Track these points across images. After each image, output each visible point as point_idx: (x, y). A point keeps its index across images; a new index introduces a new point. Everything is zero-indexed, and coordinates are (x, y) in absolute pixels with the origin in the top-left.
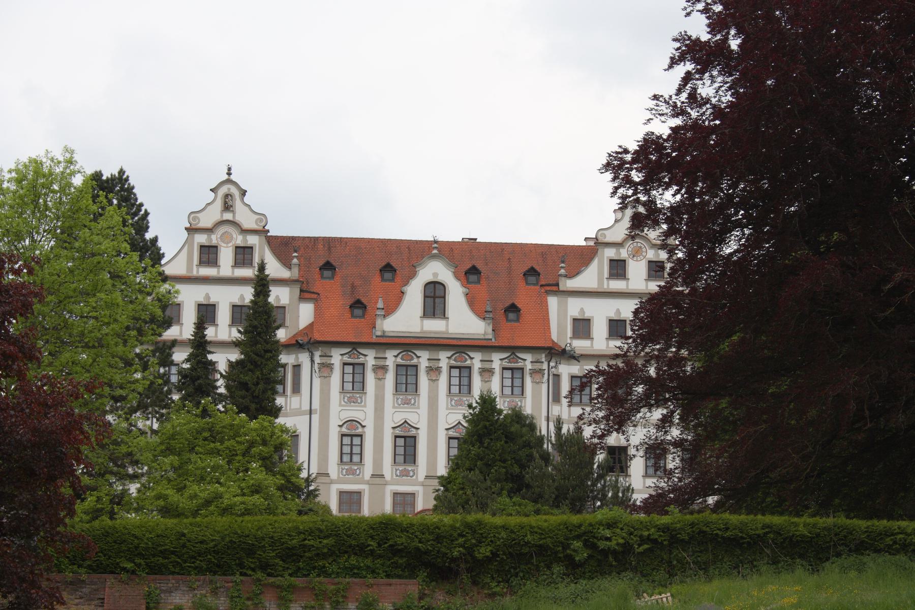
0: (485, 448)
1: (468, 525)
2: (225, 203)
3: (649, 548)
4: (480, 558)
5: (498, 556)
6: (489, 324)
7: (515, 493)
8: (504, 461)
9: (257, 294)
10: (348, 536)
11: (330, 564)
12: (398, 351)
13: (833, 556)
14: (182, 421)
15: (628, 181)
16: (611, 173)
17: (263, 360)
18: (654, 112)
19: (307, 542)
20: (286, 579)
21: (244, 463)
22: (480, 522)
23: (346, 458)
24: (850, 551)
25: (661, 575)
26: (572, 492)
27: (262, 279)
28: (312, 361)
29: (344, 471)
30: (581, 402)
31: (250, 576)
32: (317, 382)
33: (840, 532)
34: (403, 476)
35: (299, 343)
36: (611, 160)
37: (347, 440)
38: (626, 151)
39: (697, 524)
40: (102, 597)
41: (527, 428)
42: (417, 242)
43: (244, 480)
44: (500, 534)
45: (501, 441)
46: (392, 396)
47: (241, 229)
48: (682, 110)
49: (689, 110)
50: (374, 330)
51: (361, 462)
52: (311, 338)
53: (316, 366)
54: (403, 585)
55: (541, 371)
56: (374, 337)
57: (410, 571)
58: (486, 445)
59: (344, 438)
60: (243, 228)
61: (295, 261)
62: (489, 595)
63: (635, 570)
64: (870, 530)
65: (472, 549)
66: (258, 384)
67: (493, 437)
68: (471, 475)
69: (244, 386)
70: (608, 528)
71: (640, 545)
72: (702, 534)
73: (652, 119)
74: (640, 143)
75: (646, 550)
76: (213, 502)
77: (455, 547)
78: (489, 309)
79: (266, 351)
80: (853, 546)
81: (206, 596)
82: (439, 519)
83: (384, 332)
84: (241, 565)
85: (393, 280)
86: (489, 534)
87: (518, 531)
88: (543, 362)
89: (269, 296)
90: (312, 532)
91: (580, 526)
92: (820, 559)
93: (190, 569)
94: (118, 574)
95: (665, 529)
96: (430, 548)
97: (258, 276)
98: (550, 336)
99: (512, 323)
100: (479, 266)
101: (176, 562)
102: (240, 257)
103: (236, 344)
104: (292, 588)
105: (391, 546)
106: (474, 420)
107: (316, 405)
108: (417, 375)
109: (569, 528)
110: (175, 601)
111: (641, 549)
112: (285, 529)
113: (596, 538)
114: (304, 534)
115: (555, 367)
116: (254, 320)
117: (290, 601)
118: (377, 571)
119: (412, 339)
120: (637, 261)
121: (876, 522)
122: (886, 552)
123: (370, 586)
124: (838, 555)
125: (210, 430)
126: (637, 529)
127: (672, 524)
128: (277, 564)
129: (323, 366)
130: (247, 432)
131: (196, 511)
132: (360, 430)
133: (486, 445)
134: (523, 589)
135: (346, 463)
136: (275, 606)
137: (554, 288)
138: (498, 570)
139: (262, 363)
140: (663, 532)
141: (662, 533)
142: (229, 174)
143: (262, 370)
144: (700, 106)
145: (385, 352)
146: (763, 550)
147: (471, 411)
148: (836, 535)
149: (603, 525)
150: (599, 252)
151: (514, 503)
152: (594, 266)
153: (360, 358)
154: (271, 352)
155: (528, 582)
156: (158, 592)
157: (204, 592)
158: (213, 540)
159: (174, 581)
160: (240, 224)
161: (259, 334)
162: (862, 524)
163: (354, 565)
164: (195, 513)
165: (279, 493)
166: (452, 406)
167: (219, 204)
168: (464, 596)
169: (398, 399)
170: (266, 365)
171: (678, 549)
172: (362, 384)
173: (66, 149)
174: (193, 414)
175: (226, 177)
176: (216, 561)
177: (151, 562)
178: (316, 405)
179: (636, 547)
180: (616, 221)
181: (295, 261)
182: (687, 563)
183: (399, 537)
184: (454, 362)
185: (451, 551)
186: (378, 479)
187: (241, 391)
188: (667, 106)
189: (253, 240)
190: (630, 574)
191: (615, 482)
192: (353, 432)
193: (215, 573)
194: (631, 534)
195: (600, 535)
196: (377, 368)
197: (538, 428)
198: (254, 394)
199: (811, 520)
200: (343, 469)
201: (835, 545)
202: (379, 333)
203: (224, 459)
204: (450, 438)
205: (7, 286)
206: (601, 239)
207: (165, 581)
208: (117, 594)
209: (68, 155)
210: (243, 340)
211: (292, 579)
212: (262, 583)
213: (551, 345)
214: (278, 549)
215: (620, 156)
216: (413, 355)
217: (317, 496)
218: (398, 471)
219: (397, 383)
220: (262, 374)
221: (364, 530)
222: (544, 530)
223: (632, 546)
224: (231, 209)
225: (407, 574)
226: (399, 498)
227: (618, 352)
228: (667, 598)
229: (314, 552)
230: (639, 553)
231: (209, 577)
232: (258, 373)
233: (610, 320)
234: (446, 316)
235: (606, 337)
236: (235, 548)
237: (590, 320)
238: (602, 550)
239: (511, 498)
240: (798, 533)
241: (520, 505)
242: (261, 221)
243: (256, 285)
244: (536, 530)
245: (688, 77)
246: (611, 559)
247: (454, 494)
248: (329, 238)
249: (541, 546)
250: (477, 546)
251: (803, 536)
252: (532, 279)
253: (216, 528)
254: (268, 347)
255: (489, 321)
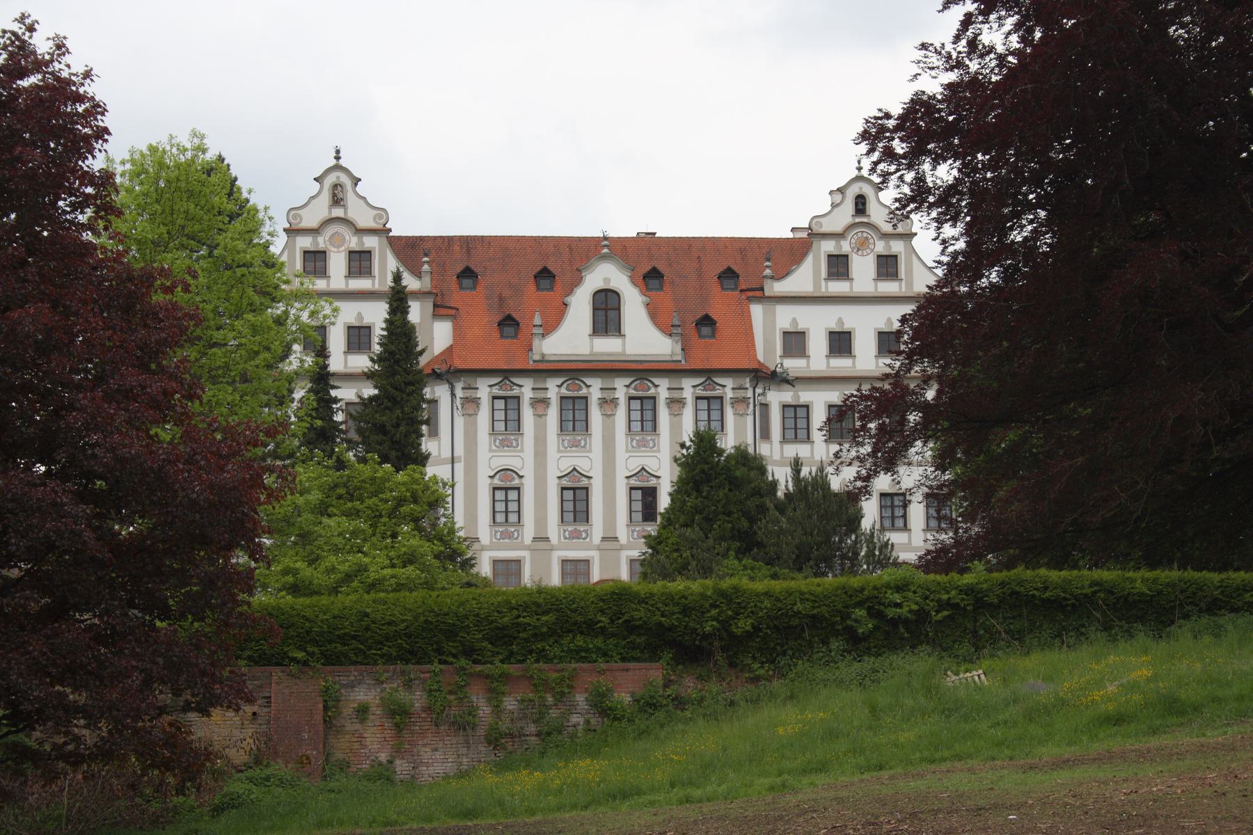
0: (704, 498)
1: (722, 593)
2: (334, 195)
3: (949, 616)
4: (739, 634)
5: (760, 630)
6: (677, 342)
7: (744, 554)
8: (729, 514)
9: (393, 311)
10: (571, 610)
11: (550, 646)
12: (562, 380)
13: (1179, 618)
14: (312, 475)
15: (889, 154)
16: (867, 144)
17: (404, 395)
18: (922, 65)
19: (521, 619)
20: (497, 667)
21: (391, 527)
22: (736, 589)
23: (500, 518)
24: (1200, 611)
25: (966, 648)
26: (817, 550)
27: (399, 292)
28: (453, 395)
29: (498, 535)
30: (796, 438)
31: (452, 663)
32: (460, 422)
33: (1188, 588)
34: (574, 538)
35: (436, 373)
36: (868, 127)
37: (500, 495)
38: (888, 116)
39: (1008, 584)
40: (267, 695)
41: (756, 472)
42: (580, 239)
43: (393, 547)
44: (762, 602)
45: (724, 489)
46: (555, 437)
47: (356, 228)
48: (958, 62)
49: (967, 62)
50: (530, 354)
51: (519, 522)
52: (451, 366)
53: (458, 402)
54: (644, 671)
55: (745, 400)
56: (531, 363)
57: (651, 653)
58: (705, 494)
59: (496, 492)
60: (358, 227)
61: (426, 267)
62: (751, 679)
63: (933, 642)
64: (1224, 584)
65: (727, 622)
66: (398, 426)
67: (713, 484)
68: (688, 532)
69: (381, 429)
70: (897, 592)
71: (938, 612)
72: (1015, 596)
73: (920, 75)
74: (905, 106)
75: (945, 618)
76: (356, 576)
77: (707, 621)
78: (677, 323)
79: (408, 384)
80: (1203, 605)
81: (397, 691)
82: (685, 587)
83: (543, 355)
84: (439, 651)
85: (551, 289)
86: (749, 603)
87: (786, 599)
88: (747, 389)
89: (407, 313)
90: (527, 607)
91: (862, 590)
92: (1162, 622)
93: (376, 657)
94: (286, 665)
95: (969, 590)
96: (676, 623)
97: (393, 288)
98: (756, 355)
99: (707, 340)
100: (661, 268)
101: (357, 648)
102: (311, 266)
103: (368, 376)
104: (505, 678)
105: (626, 621)
106: (688, 463)
107: (460, 451)
108: (587, 409)
109: (849, 593)
110: (358, 698)
111: (940, 616)
112: (492, 604)
113: (883, 604)
114: (517, 609)
115: (763, 394)
116: (390, 344)
117: (503, 693)
118: (610, 653)
119: (579, 363)
120: (863, 255)
121: (1232, 574)
122: (1247, 611)
123: (602, 672)
124: (1186, 616)
125: (345, 486)
126: (934, 591)
127: (977, 584)
128: (485, 648)
129: (466, 400)
130: (394, 487)
131: (334, 588)
132: (516, 482)
133: (705, 494)
134: (794, 671)
135: (500, 524)
136: (484, 701)
137: (758, 294)
138: (760, 648)
139: (402, 399)
140: (967, 594)
141: (965, 597)
142: (338, 158)
143: (402, 408)
144: (982, 56)
145: (545, 381)
146: (1091, 613)
147: (684, 451)
148: (1182, 592)
149: (891, 589)
150: (814, 245)
151: (744, 566)
152: (808, 264)
153: (513, 390)
154: (413, 385)
155: (800, 662)
156: (337, 687)
157: (395, 685)
158: (403, 621)
159: (356, 673)
160: (354, 222)
161: (397, 362)
162: (1215, 577)
163: (581, 646)
164: (335, 590)
165: (436, 563)
166: (633, 447)
167: (326, 197)
168: (720, 682)
169: (563, 440)
170: (407, 401)
171: (985, 615)
172: (517, 423)
173: (194, 134)
174: (326, 466)
175: (334, 162)
176: (408, 647)
177: (327, 650)
178: (460, 451)
179: (934, 614)
180: (834, 206)
181: (426, 267)
182: (996, 632)
183: (637, 610)
184: (633, 392)
185: (701, 626)
186: (542, 543)
187: (378, 435)
188: (939, 57)
189: (371, 242)
190: (927, 648)
191: (870, 537)
192: (508, 484)
193: (407, 662)
194: (926, 598)
195: (887, 601)
196: (736, 402)
197: (770, 472)
198: (394, 439)
199: (1150, 575)
200: (496, 532)
201: (1181, 605)
202: (537, 357)
203: (365, 521)
204: (631, 489)
205: (155, 307)
206: (816, 229)
207: (346, 674)
208: (286, 691)
209: (196, 141)
210: (377, 370)
211: (505, 666)
212: (467, 672)
213: (756, 366)
214: (485, 630)
215: (880, 122)
216: (582, 384)
217: (473, 566)
218: (567, 533)
219: (561, 421)
220: (403, 412)
221: (593, 602)
222: (818, 596)
223: (928, 614)
224: (342, 203)
225: (647, 656)
226: (569, 567)
227: (888, 370)
228: (979, 676)
229: (530, 632)
230: (936, 622)
231: (400, 666)
232: (398, 412)
233: (830, 333)
234: (622, 333)
235: (825, 354)
236: (431, 629)
237: (804, 333)
238: (891, 618)
239: (740, 560)
240: (1135, 591)
241: (752, 569)
242: (381, 217)
243: (391, 299)
244: (807, 596)
245: (967, 21)
246: (902, 630)
247: (667, 557)
248: (467, 236)
249: (814, 617)
250: (734, 619)
251: (1142, 594)
252: (729, 283)
253: (407, 606)
254: (410, 378)
255: (676, 338)
